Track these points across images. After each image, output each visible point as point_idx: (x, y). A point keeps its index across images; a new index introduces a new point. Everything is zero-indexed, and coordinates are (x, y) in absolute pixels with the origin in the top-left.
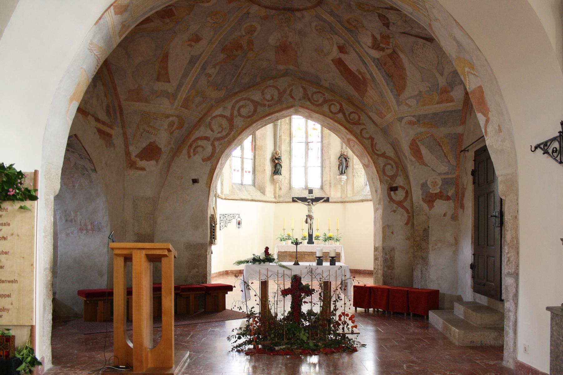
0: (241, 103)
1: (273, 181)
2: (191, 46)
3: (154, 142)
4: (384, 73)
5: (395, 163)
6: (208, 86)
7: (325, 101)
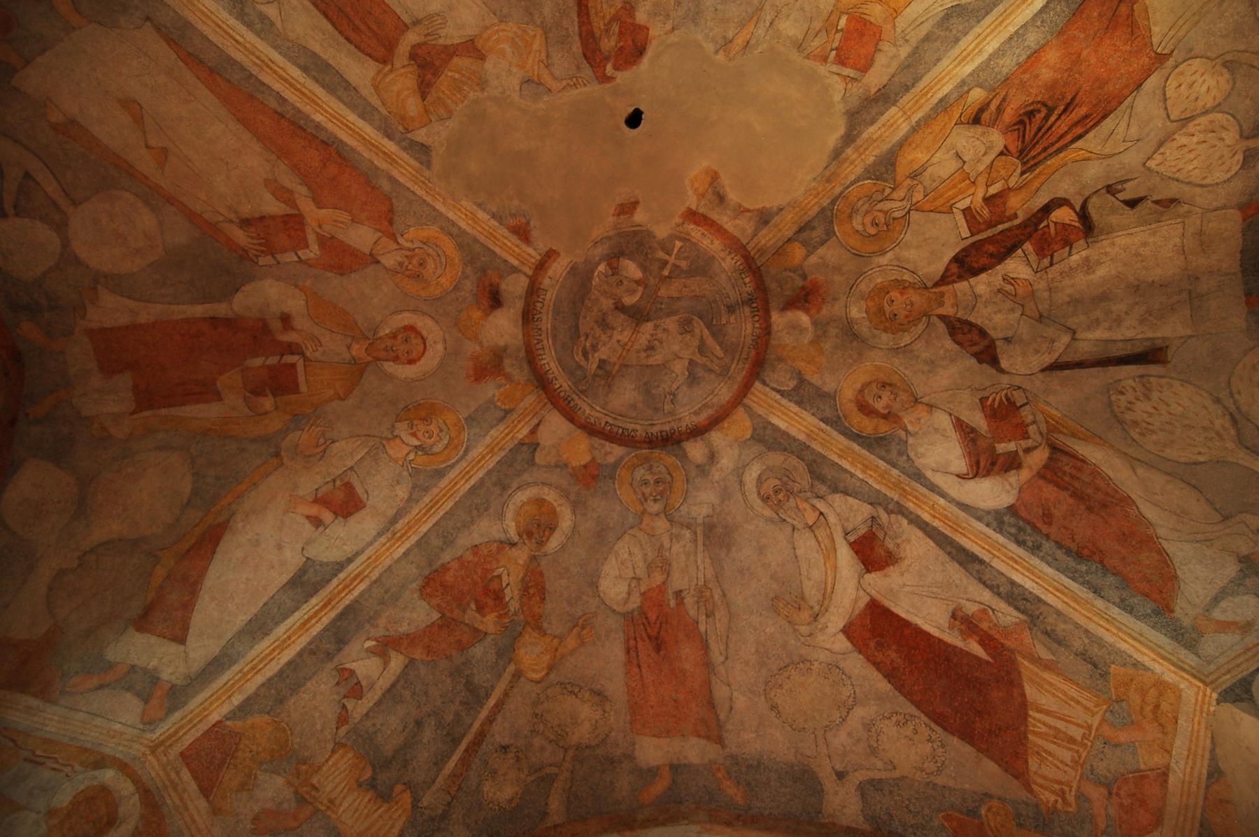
2: (317, 522)
4: (1060, 554)
6: (338, 745)
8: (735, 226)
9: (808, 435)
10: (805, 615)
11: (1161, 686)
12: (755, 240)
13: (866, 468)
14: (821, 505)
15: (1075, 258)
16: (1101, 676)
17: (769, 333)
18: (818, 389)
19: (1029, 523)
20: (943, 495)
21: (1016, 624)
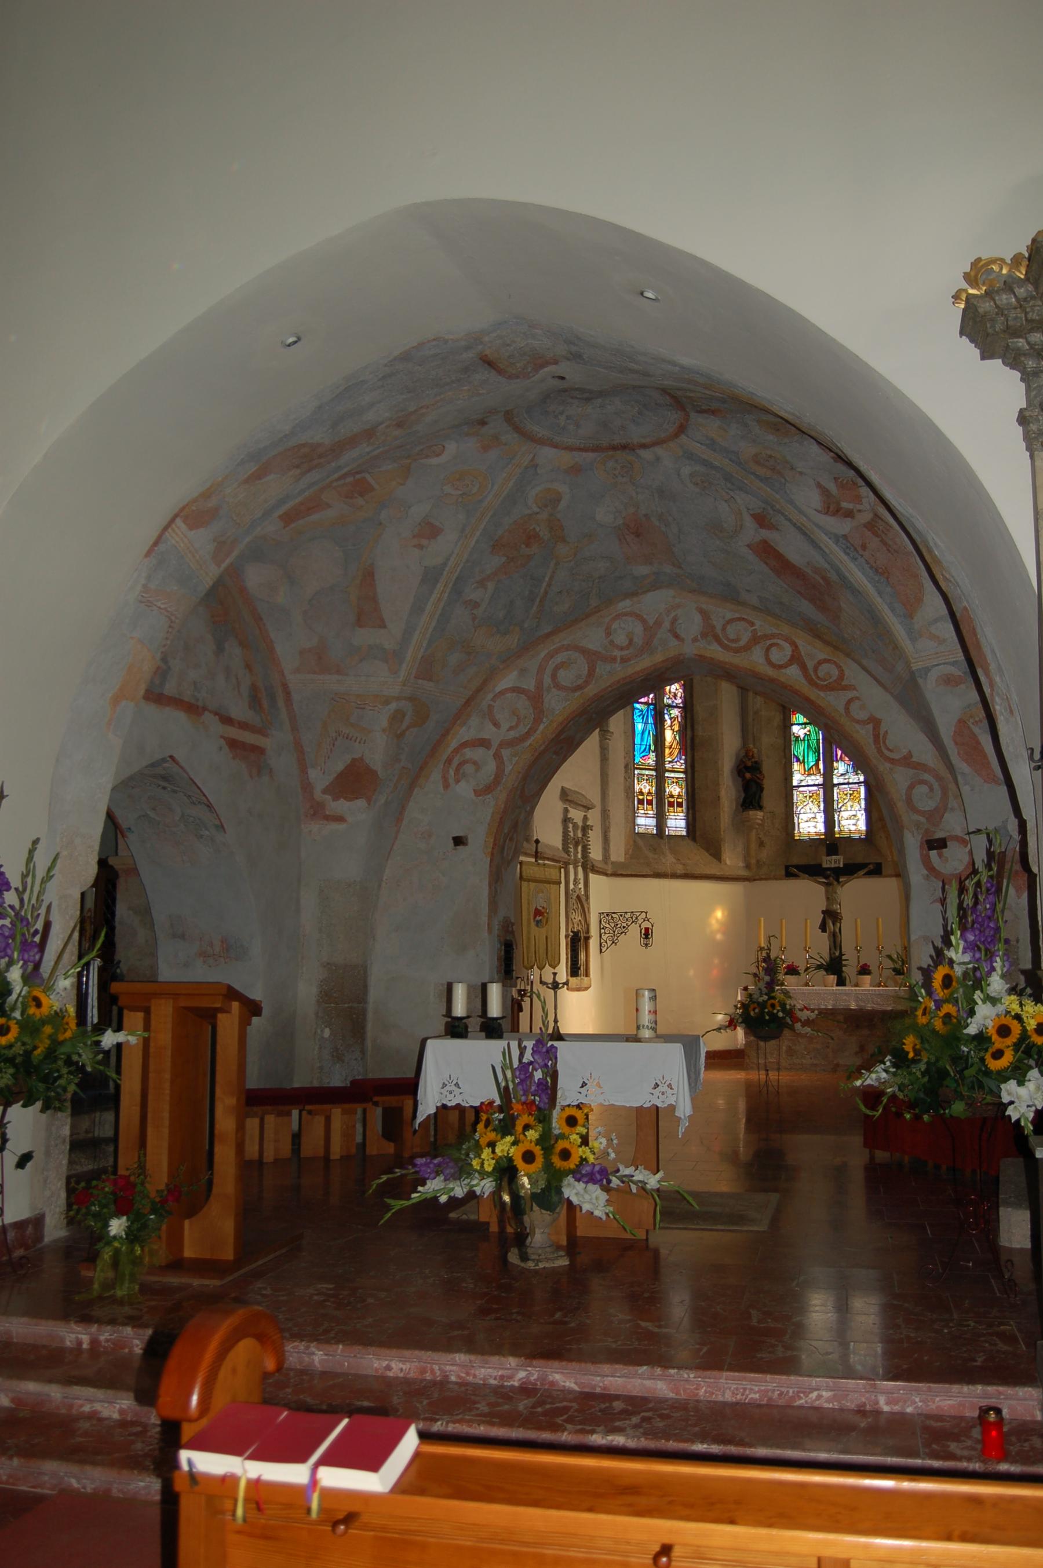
0: (559, 658)
1: (741, 826)
2: (421, 547)
3: (362, 759)
5: (939, 778)
7: (755, 640)
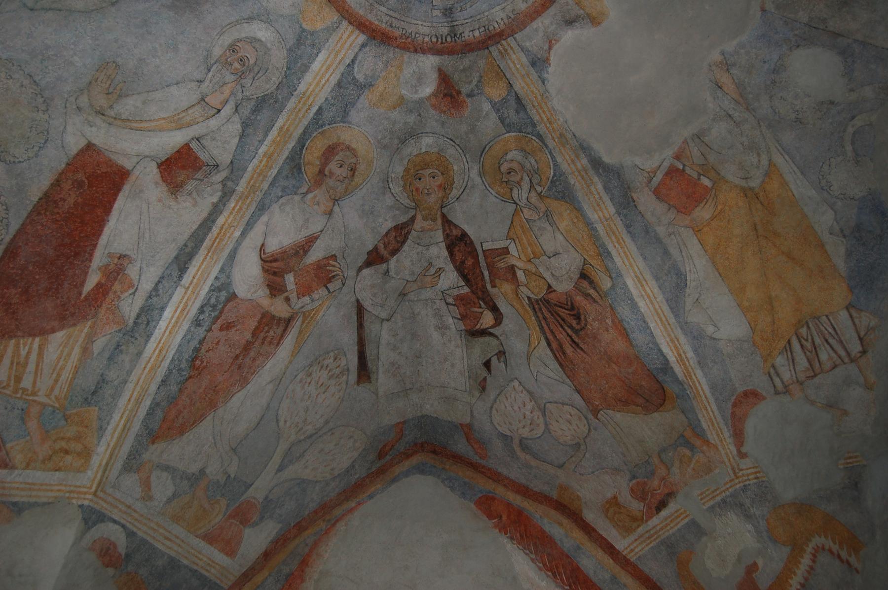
4: (194, 343)
8: (536, 30)
9: (304, 93)
10: (102, 101)
11: (86, 454)
12: (516, 48)
13: (269, 156)
14: (228, 109)
15: (451, 320)
16: (86, 399)
17: (416, 51)
18: (353, 104)
19: (221, 313)
20: (244, 234)
21: (123, 317)
